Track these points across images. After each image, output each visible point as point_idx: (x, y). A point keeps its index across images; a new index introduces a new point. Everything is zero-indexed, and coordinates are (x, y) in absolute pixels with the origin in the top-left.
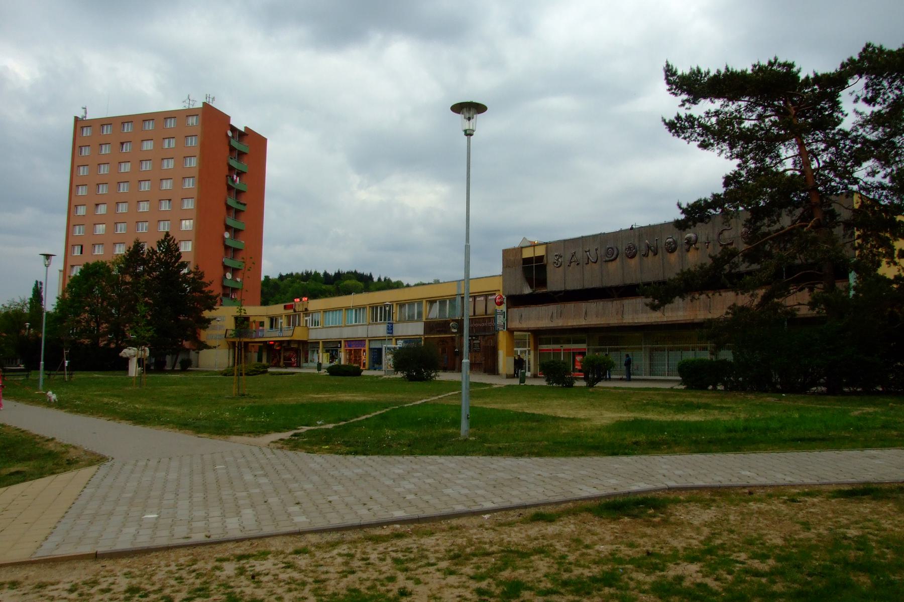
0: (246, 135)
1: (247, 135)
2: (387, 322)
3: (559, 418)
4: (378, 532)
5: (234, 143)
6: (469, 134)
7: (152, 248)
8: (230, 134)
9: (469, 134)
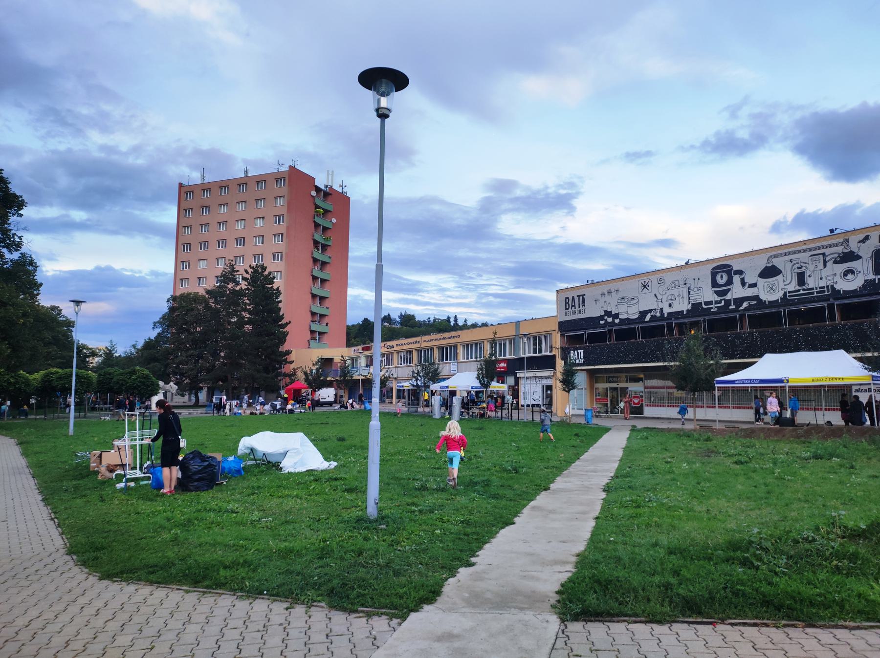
0: (327, 194)
1: (331, 194)
2: (478, 359)
3: (276, 594)
4: (862, 387)
5: (319, 202)
6: (383, 115)
7: (456, 317)
8: (314, 193)
9: (383, 115)
